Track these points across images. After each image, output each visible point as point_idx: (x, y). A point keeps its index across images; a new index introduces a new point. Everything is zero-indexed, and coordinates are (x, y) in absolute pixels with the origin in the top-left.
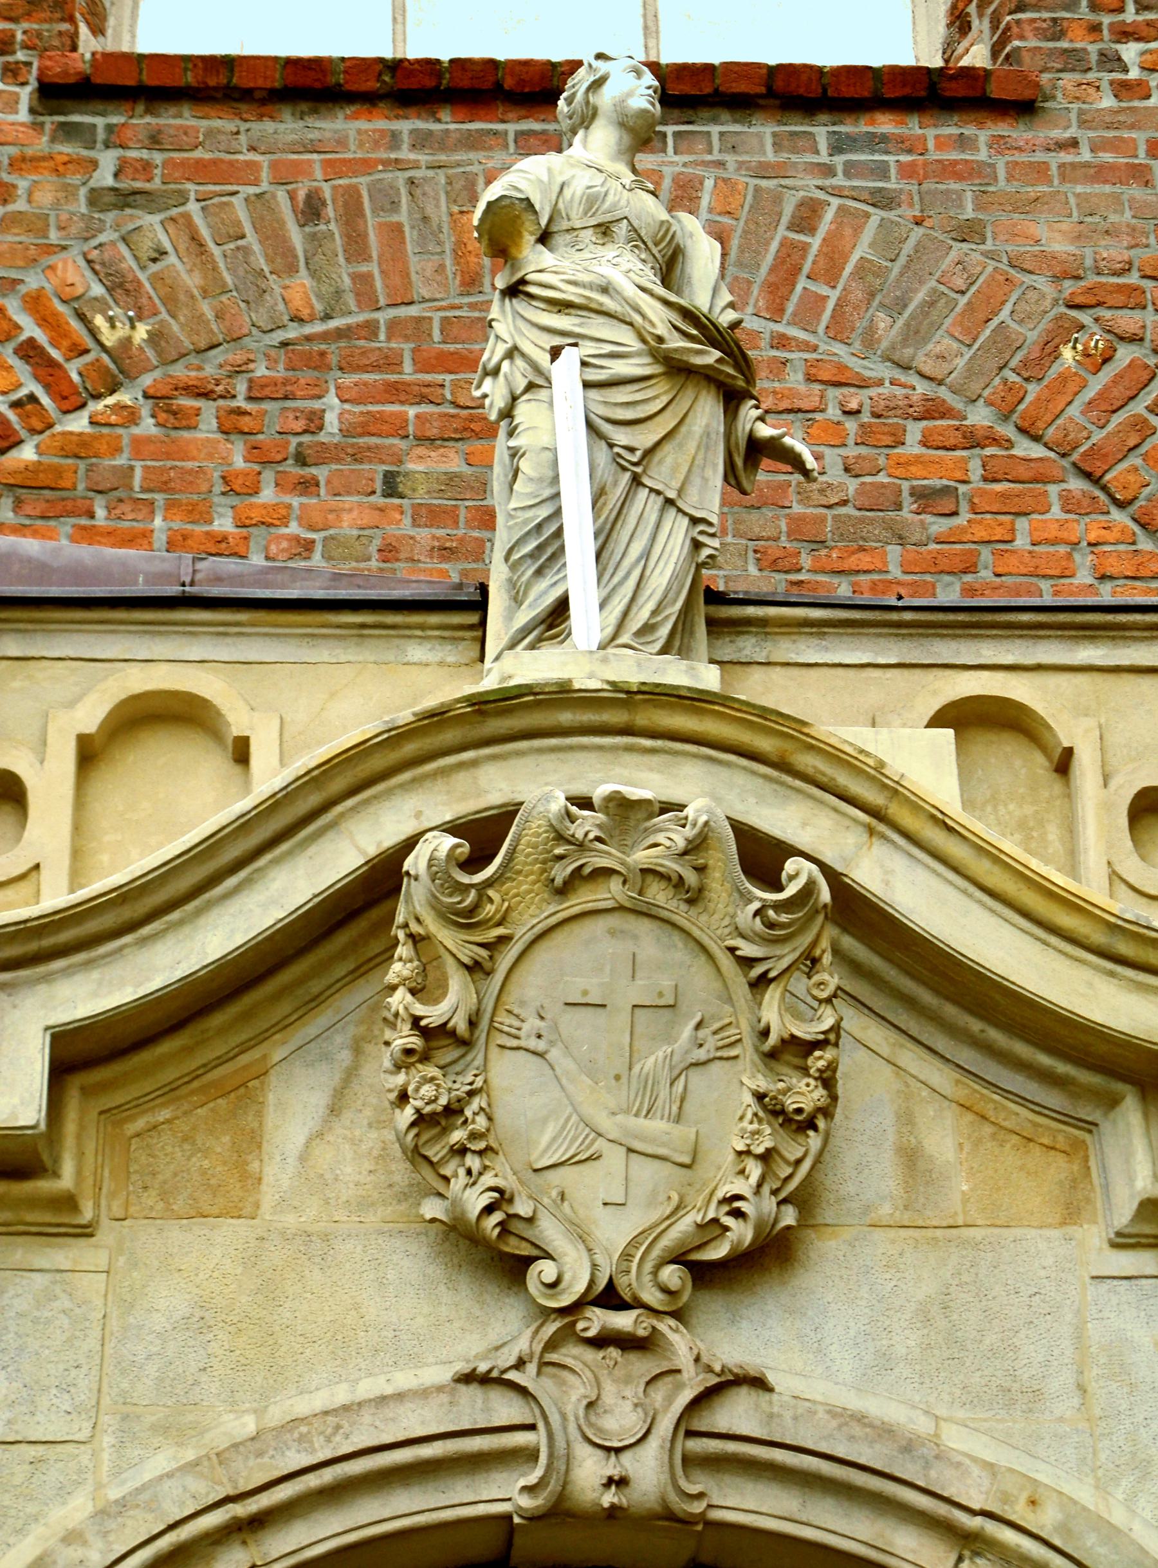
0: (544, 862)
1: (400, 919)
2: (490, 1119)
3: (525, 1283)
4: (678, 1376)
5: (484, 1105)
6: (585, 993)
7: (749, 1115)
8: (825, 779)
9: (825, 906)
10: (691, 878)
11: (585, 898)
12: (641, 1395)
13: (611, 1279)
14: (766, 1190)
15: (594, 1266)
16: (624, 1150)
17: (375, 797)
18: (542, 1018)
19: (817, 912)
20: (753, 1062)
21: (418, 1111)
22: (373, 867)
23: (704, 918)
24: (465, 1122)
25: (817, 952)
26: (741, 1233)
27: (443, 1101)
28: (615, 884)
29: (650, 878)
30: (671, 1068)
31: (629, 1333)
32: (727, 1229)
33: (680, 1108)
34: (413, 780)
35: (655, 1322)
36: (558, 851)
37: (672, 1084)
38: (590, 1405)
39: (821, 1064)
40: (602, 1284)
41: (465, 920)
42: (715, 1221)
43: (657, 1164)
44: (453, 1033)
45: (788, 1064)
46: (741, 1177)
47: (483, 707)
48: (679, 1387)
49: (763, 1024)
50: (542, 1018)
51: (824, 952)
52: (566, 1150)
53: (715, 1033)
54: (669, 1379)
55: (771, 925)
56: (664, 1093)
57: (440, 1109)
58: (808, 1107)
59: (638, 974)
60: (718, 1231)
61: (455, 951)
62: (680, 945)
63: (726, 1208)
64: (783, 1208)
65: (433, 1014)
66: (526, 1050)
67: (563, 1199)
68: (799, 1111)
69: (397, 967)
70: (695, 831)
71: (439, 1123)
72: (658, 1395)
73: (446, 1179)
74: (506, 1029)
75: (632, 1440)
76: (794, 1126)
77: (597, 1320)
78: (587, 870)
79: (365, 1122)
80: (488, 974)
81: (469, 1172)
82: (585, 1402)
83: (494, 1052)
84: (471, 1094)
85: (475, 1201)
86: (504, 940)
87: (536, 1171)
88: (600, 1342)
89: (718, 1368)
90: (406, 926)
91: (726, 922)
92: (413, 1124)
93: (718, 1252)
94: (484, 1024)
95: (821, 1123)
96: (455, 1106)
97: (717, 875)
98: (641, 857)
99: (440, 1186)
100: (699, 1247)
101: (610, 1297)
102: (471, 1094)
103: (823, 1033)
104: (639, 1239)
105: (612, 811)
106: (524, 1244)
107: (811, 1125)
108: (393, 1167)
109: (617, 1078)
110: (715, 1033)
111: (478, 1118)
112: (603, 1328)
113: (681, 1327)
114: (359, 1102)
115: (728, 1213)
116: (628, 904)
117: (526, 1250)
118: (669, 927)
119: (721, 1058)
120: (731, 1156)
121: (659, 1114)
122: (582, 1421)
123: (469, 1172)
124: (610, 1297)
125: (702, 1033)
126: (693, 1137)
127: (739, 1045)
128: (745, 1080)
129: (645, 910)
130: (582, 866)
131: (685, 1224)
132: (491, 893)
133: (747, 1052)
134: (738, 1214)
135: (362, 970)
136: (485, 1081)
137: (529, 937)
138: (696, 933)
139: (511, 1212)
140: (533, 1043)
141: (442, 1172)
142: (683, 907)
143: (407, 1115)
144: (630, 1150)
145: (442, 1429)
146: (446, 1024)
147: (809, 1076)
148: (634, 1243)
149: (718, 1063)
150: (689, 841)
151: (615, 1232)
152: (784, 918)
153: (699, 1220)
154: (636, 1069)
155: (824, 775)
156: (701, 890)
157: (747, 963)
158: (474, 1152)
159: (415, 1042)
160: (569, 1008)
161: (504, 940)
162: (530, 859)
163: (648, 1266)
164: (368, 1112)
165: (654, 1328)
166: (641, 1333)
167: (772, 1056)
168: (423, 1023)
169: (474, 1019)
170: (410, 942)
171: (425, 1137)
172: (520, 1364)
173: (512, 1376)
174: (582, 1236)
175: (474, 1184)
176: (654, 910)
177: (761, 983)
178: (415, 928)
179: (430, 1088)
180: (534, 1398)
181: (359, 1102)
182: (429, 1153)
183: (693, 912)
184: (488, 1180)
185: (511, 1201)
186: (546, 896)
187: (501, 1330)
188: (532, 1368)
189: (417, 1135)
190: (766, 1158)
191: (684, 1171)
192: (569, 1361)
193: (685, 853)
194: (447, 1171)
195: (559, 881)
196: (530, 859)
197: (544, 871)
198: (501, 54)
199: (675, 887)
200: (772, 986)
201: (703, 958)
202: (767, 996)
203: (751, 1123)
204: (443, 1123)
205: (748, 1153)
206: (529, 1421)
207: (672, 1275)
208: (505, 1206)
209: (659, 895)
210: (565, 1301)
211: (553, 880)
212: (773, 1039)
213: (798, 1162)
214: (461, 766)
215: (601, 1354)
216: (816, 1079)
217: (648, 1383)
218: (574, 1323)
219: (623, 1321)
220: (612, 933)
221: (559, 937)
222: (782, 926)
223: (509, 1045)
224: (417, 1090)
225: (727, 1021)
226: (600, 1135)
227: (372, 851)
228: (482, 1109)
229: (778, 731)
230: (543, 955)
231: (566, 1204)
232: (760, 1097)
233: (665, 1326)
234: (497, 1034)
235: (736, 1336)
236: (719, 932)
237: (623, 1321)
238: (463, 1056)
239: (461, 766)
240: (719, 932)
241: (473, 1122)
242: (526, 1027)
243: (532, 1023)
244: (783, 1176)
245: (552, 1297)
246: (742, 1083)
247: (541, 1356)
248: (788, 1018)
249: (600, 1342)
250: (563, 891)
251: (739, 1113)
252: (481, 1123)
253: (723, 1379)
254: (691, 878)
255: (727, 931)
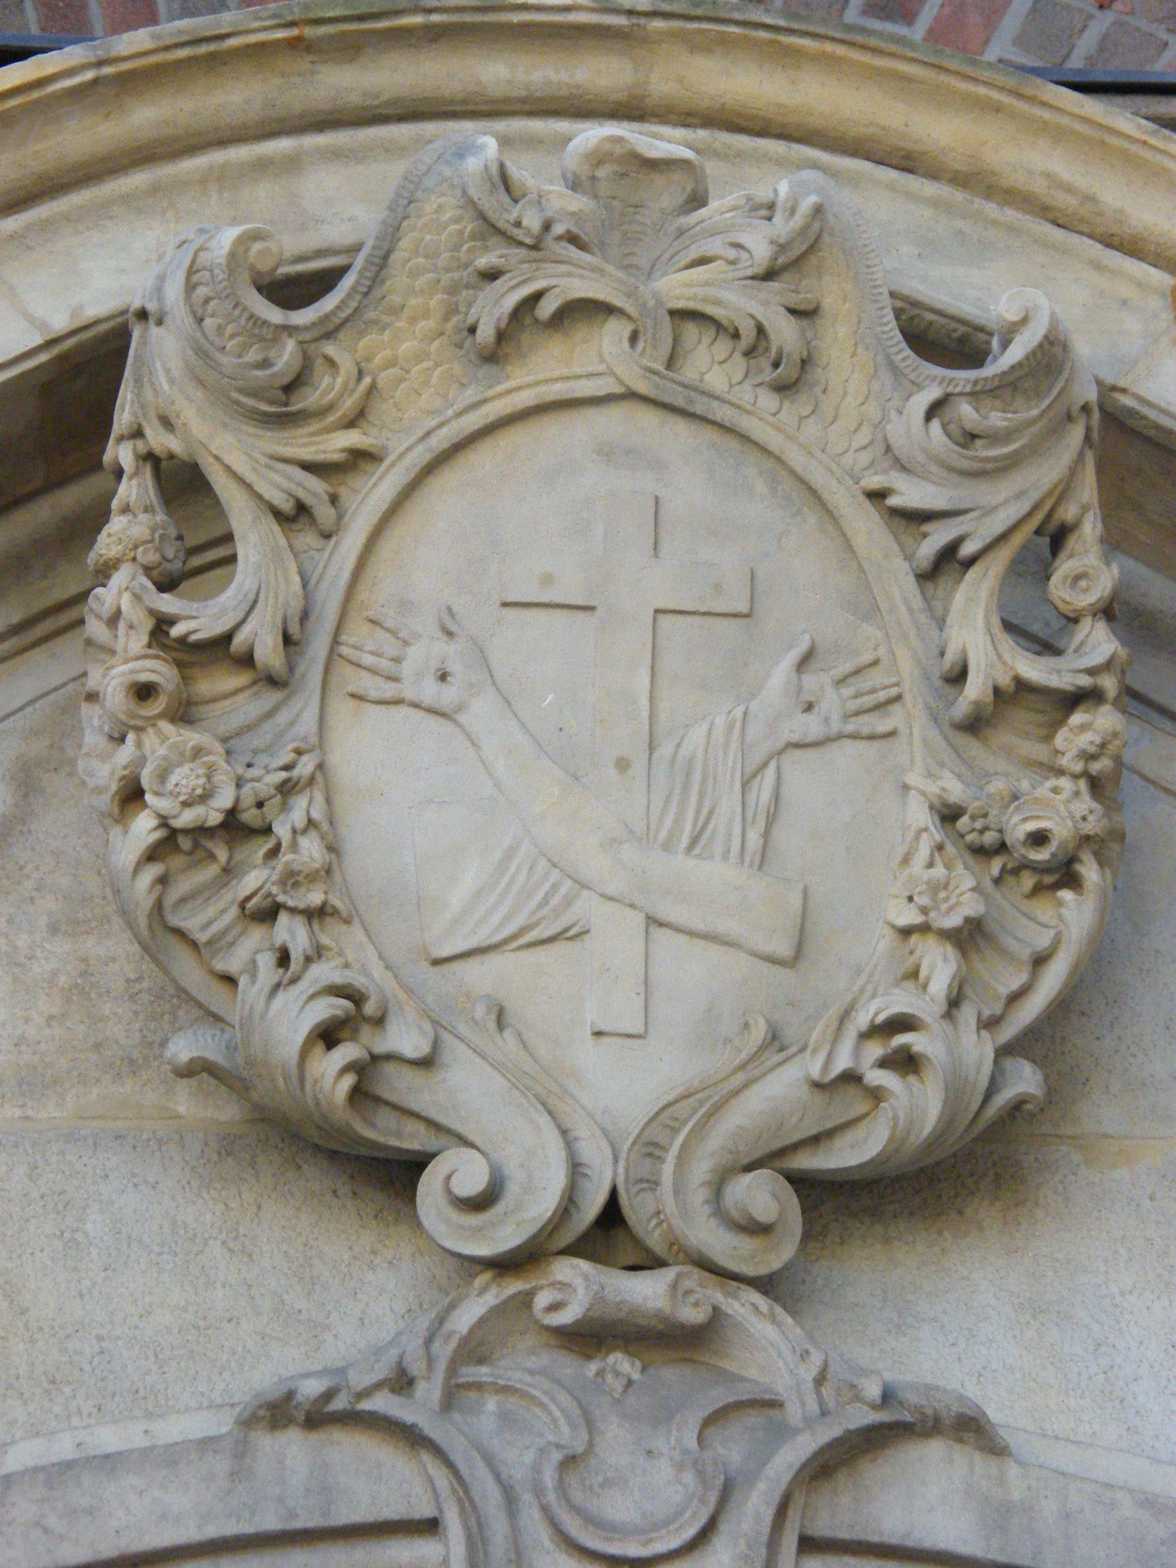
0: (453, 290)
1: (123, 418)
2: (332, 849)
3: (411, 1197)
4: (774, 1413)
5: (316, 814)
6: (547, 580)
7: (924, 851)
8: (1071, 201)
9: (1085, 408)
10: (785, 332)
11: (547, 368)
12: (693, 1444)
13: (614, 1193)
14: (968, 1014)
15: (576, 1169)
16: (640, 918)
17: (67, 217)
18: (450, 634)
19: (1069, 418)
20: (925, 742)
21: (164, 822)
22: (62, 358)
23: (812, 429)
24: (274, 852)
25: (1069, 512)
26: (914, 1111)
27: (224, 800)
28: (610, 338)
29: (691, 330)
30: (744, 750)
31: (659, 1315)
32: (877, 1095)
33: (766, 835)
34: (155, 189)
35: (719, 1298)
36: (484, 261)
37: (745, 786)
38: (570, 1462)
39: (1086, 740)
40: (592, 1206)
41: (281, 404)
42: (851, 1078)
43: (714, 950)
44: (247, 660)
45: (1008, 751)
46: (910, 984)
47: (309, 32)
48: (782, 1432)
49: (950, 657)
50: (450, 634)
51: (1085, 509)
52: (507, 918)
53: (841, 682)
54: (754, 1419)
55: (970, 437)
56: (729, 803)
57: (215, 818)
58: (1061, 831)
59: (665, 547)
60: (861, 1107)
61: (250, 477)
62: (761, 487)
63: (875, 1050)
64: (1008, 1063)
65: (199, 618)
66: (415, 705)
67: (500, 1023)
68: (1039, 839)
69: (117, 524)
70: (797, 221)
71: (212, 857)
72: (732, 1448)
73: (229, 980)
74: (368, 660)
75: (674, 1543)
76: (1028, 881)
77: (575, 1288)
78: (546, 308)
79: (43, 921)
80: (327, 536)
81: (284, 959)
82: (557, 1456)
83: (342, 709)
84: (287, 789)
85: (292, 1017)
86: (360, 458)
87: (437, 962)
88: (590, 1337)
89: (873, 1390)
90: (137, 433)
91: (863, 437)
92: (152, 855)
93: (849, 1154)
94: (318, 648)
95: (1090, 871)
96: (249, 816)
97: (842, 332)
98: (677, 286)
99: (216, 997)
100: (815, 1140)
101: (608, 1232)
102: (287, 789)
103: (1091, 672)
104: (683, 1108)
105: (604, 189)
106: (411, 1126)
107: (1065, 875)
108: (107, 1009)
109: (623, 765)
110: (841, 682)
111: (304, 842)
112: (599, 1299)
113: (779, 1310)
114: (29, 884)
115: (883, 1063)
116: (642, 387)
117: (413, 1139)
118: (734, 444)
119: (854, 736)
120: (885, 942)
121: (718, 850)
122: (551, 1497)
123: (284, 959)
124: (608, 1232)
125: (811, 681)
126: (796, 900)
127: (896, 708)
128: (913, 779)
129: (680, 402)
130: (537, 296)
131: (780, 1091)
132: (330, 349)
133: (914, 721)
134: (906, 1062)
135: (39, 631)
136: (320, 766)
137: (420, 456)
138: (795, 458)
139: (380, 1048)
140: (429, 691)
141: (219, 966)
142: (768, 401)
143: (143, 828)
144: (654, 921)
145: (212, 1531)
146: (227, 638)
147: (1061, 772)
148: (664, 1116)
149: (850, 747)
150: (782, 248)
151: (622, 1089)
152: (997, 419)
153: (815, 1070)
154: (665, 750)
155: (1069, 189)
156: (805, 363)
157: (918, 518)
158: (293, 911)
159: (159, 671)
160: (511, 613)
161: (360, 458)
162: (420, 282)
163: (701, 1169)
164: (49, 904)
165: (716, 1310)
166: (692, 1315)
167: (974, 725)
168: (176, 631)
169: (294, 629)
170: (148, 471)
171: (183, 885)
172: (402, 1382)
173: (381, 1403)
174: (547, 1097)
175: (294, 981)
176: (701, 406)
177: (949, 562)
178: (158, 439)
179: (187, 774)
180: (438, 1451)
181: (29, 884)
182: (191, 922)
183: (790, 412)
184: (324, 973)
185: (379, 1021)
186: (457, 368)
187: (352, 1297)
188: (429, 1391)
189: (163, 880)
190: (970, 937)
191: (781, 971)
192: (517, 1378)
193: (769, 275)
194: (232, 963)
195: (486, 333)
196: (420, 282)
197: (451, 311)
198: (228, 1534)
199: (749, 353)
200: (972, 574)
201: (812, 519)
202: (959, 597)
203: (930, 865)
204: (222, 854)
205: (925, 928)
206: (424, 1511)
207: (761, 1195)
208: (366, 1032)
209: (711, 367)
210: (505, 1235)
211: (472, 330)
212: (975, 689)
213: (1040, 961)
214: (262, 166)
215: (592, 1368)
216: (1076, 777)
217: (707, 1422)
218: (526, 1300)
219: (646, 1292)
220: (607, 453)
221: (485, 457)
222: (995, 438)
223: (373, 694)
224: (163, 776)
225: (867, 658)
226: (584, 886)
227: (60, 322)
228: (311, 823)
229: (966, 96)
230: (448, 497)
231: (507, 1033)
232: (949, 815)
233: (745, 1307)
234: (348, 670)
235: (944, 1319)
236: (848, 460)
237: (646, 1292)
238: (270, 714)
239: (262, 166)
240: (848, 460)
241: (294, 846)
242: (415, 655)
243: (425, 652)
244: (1004, 991)
245: (476, 1232)
246: (906, 787)
247: (452, 1370)
248: (1007, 643)
249: (590, 1337)
250: (498, 351)
251: (900, 851)
252: (311, 850)
253: (883, 1417)
254: (785, 332)
255: (865, 458)
